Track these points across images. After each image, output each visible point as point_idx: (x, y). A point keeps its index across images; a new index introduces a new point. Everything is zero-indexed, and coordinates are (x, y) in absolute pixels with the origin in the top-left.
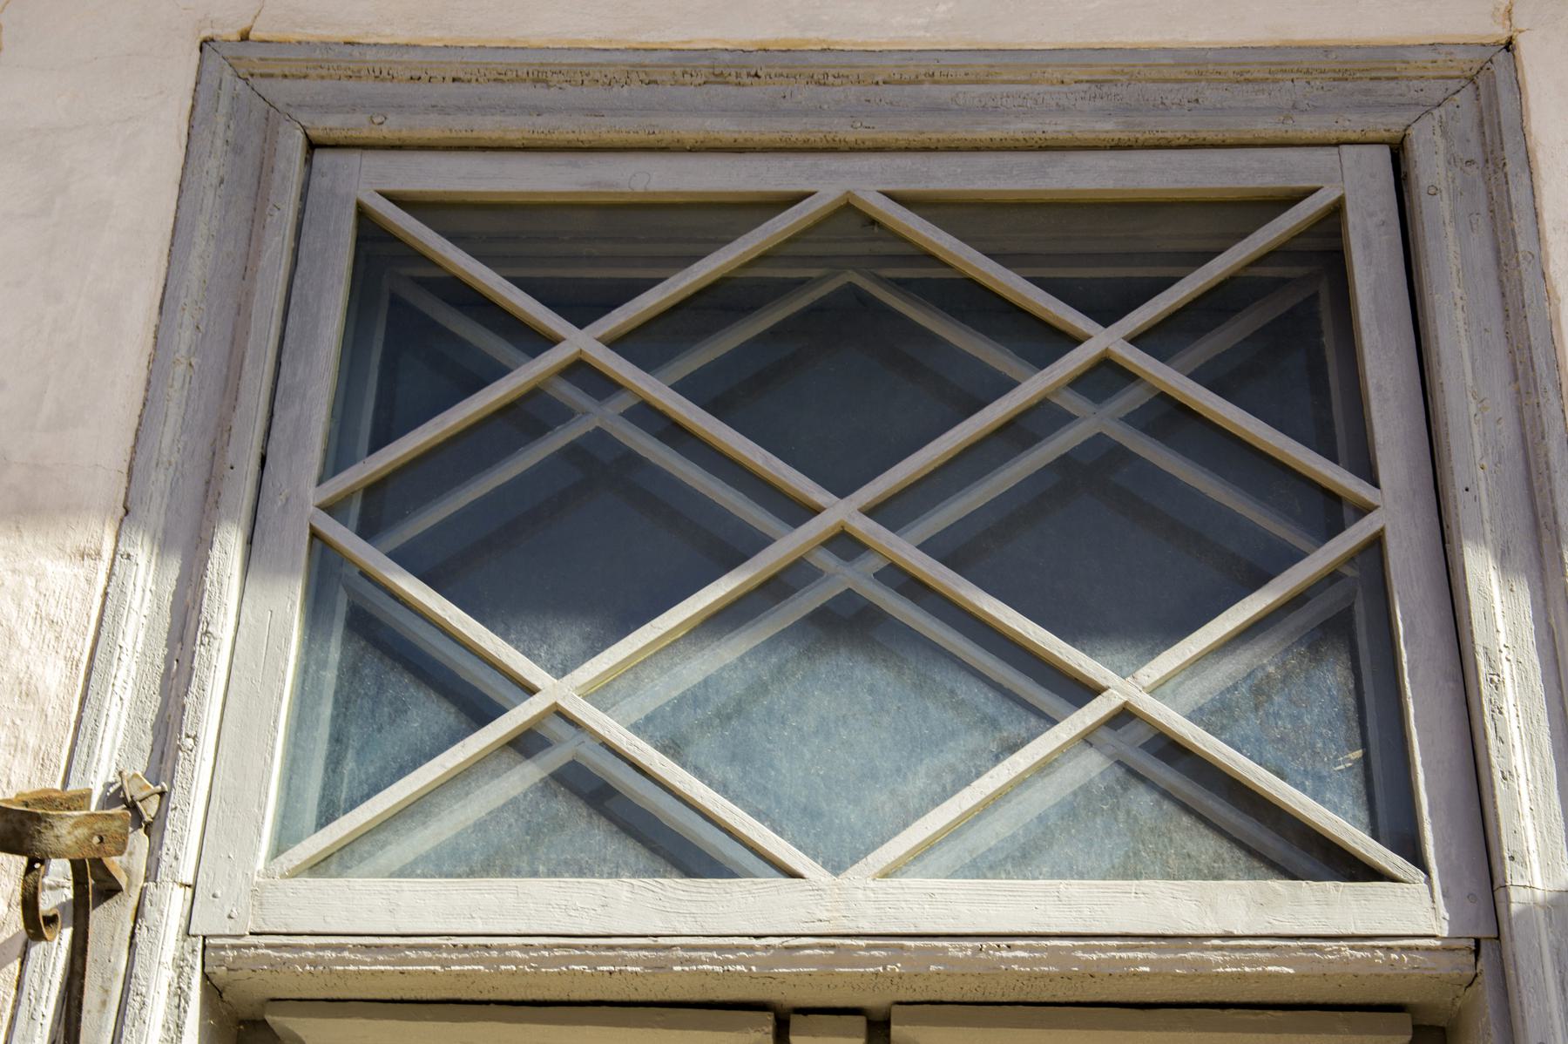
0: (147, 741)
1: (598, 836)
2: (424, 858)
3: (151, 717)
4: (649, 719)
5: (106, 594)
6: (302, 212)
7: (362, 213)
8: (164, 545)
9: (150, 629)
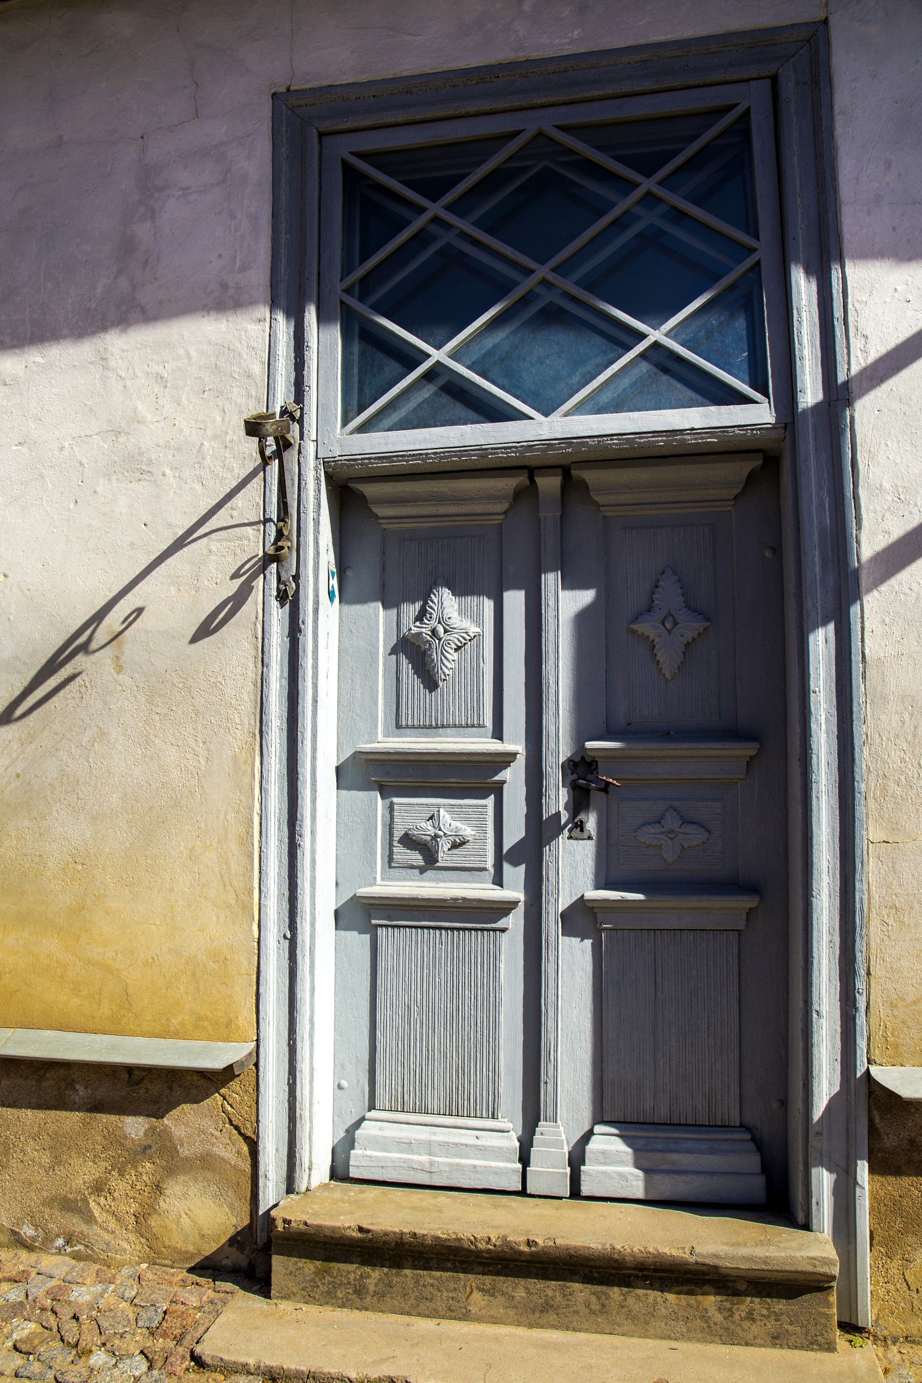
0: (293, 389)
1: (459, 410)
2: (396, 424)
3: (293, 380)
4: (474, 363)
5: (270, 335)
6: (320, 165)
7: (344, 163)
8: (288, 315)
9: (288, 346)
